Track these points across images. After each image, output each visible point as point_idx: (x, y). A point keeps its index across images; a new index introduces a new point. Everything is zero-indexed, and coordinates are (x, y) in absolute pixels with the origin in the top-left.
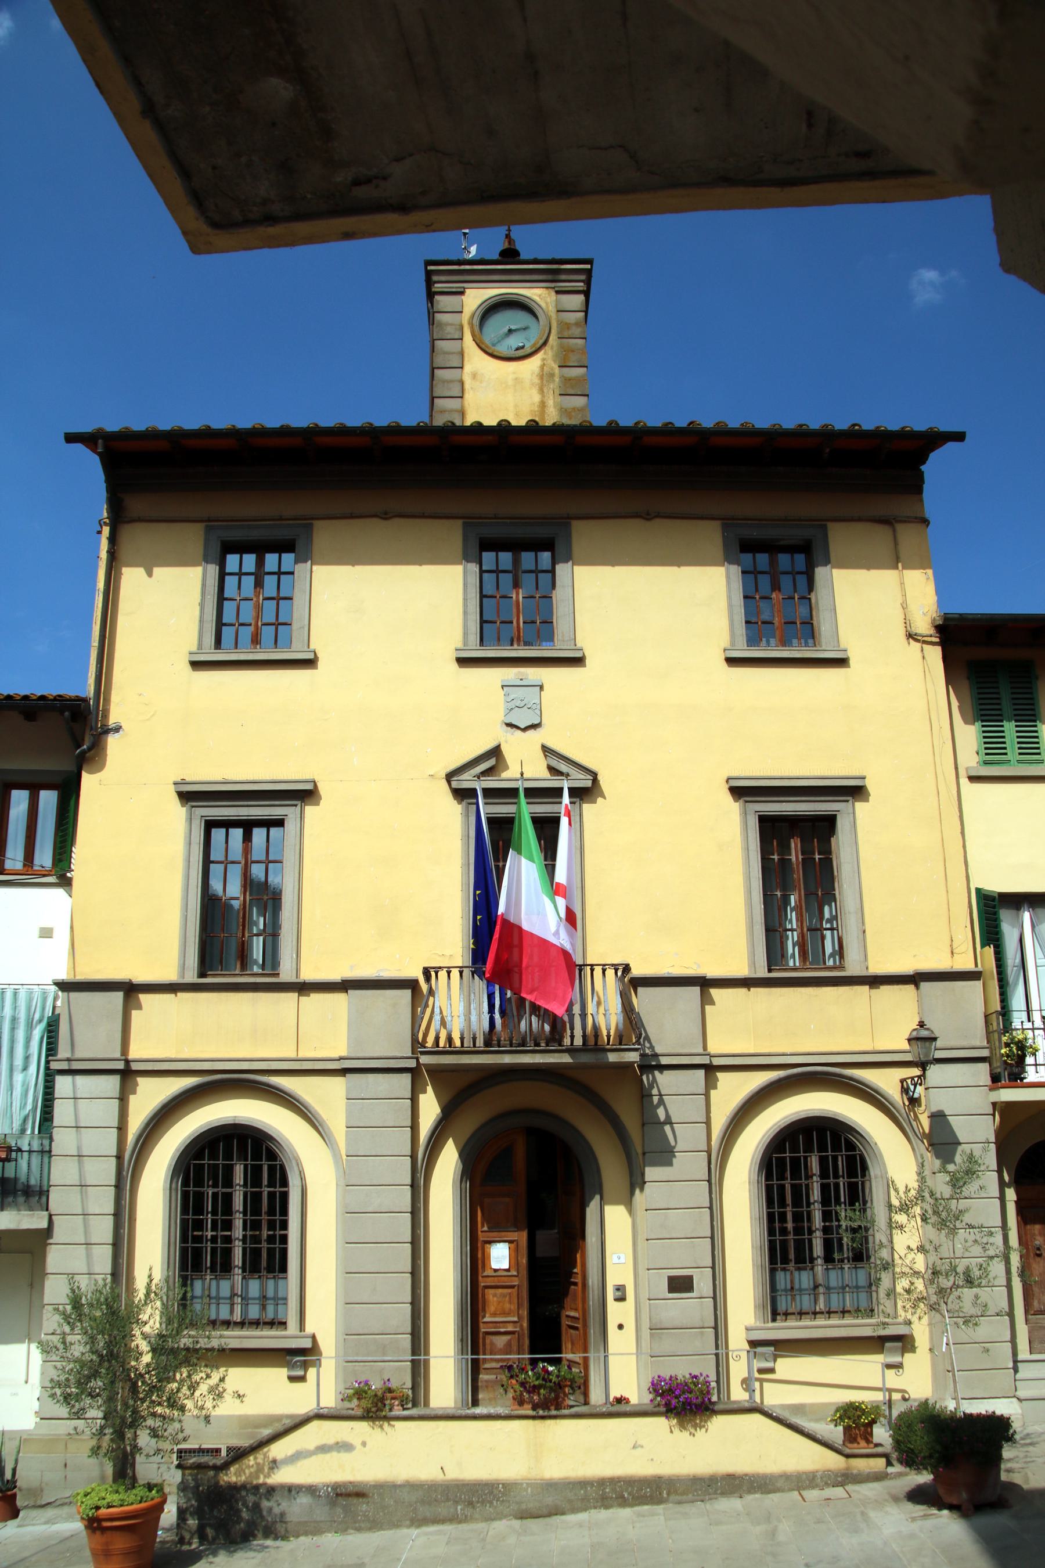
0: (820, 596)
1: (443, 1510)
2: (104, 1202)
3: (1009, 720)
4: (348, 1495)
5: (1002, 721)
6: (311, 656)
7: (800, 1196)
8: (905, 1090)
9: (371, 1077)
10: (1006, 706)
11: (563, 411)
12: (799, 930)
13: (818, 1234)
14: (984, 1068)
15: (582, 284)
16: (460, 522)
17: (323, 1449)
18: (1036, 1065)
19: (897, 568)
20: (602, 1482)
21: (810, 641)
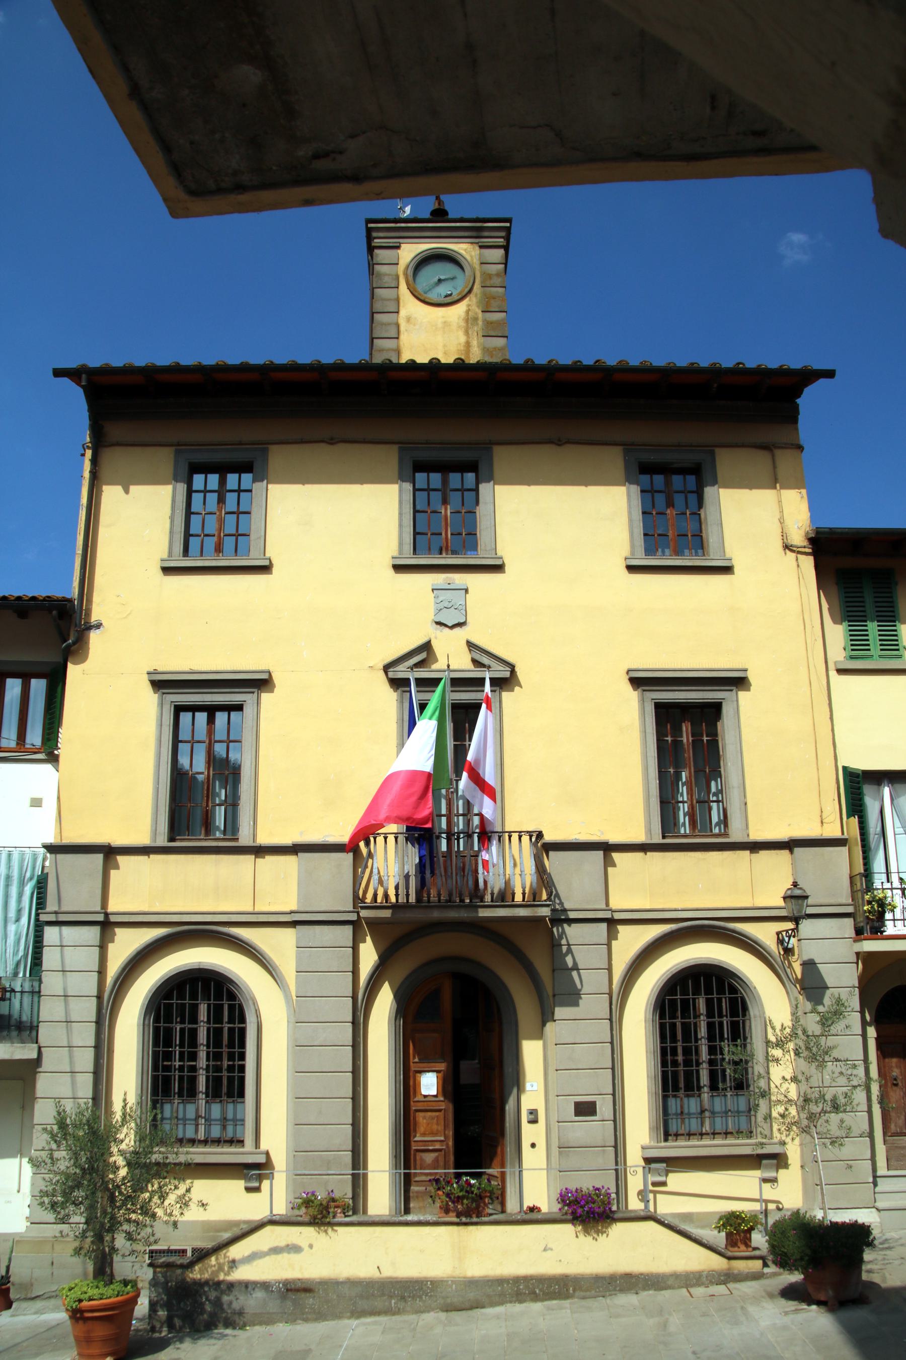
0: (709, 512)
1: (379, 1304)
2: (86, 1035)
3: (872, 621)
4: (298, 1290)
5: (866, 621)
6: (266, 563)
7: (689, 1033)
8: (780, 941)
9: (318, 928)
10: (870, 607)
11: (485, 350)
12: (689, 802)
13: (705, 1065)
14: (849, 923)
15: (502, 240)
16: (395, 448)
17: (276, 1250)
18: (894, 920)
19: (775, 488)
20: (527, 1279)
21: (700, 551)
